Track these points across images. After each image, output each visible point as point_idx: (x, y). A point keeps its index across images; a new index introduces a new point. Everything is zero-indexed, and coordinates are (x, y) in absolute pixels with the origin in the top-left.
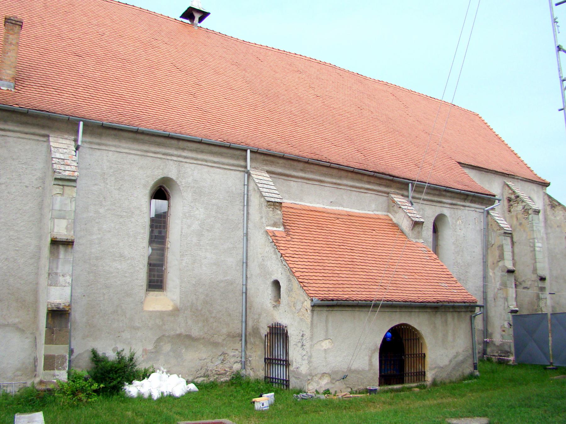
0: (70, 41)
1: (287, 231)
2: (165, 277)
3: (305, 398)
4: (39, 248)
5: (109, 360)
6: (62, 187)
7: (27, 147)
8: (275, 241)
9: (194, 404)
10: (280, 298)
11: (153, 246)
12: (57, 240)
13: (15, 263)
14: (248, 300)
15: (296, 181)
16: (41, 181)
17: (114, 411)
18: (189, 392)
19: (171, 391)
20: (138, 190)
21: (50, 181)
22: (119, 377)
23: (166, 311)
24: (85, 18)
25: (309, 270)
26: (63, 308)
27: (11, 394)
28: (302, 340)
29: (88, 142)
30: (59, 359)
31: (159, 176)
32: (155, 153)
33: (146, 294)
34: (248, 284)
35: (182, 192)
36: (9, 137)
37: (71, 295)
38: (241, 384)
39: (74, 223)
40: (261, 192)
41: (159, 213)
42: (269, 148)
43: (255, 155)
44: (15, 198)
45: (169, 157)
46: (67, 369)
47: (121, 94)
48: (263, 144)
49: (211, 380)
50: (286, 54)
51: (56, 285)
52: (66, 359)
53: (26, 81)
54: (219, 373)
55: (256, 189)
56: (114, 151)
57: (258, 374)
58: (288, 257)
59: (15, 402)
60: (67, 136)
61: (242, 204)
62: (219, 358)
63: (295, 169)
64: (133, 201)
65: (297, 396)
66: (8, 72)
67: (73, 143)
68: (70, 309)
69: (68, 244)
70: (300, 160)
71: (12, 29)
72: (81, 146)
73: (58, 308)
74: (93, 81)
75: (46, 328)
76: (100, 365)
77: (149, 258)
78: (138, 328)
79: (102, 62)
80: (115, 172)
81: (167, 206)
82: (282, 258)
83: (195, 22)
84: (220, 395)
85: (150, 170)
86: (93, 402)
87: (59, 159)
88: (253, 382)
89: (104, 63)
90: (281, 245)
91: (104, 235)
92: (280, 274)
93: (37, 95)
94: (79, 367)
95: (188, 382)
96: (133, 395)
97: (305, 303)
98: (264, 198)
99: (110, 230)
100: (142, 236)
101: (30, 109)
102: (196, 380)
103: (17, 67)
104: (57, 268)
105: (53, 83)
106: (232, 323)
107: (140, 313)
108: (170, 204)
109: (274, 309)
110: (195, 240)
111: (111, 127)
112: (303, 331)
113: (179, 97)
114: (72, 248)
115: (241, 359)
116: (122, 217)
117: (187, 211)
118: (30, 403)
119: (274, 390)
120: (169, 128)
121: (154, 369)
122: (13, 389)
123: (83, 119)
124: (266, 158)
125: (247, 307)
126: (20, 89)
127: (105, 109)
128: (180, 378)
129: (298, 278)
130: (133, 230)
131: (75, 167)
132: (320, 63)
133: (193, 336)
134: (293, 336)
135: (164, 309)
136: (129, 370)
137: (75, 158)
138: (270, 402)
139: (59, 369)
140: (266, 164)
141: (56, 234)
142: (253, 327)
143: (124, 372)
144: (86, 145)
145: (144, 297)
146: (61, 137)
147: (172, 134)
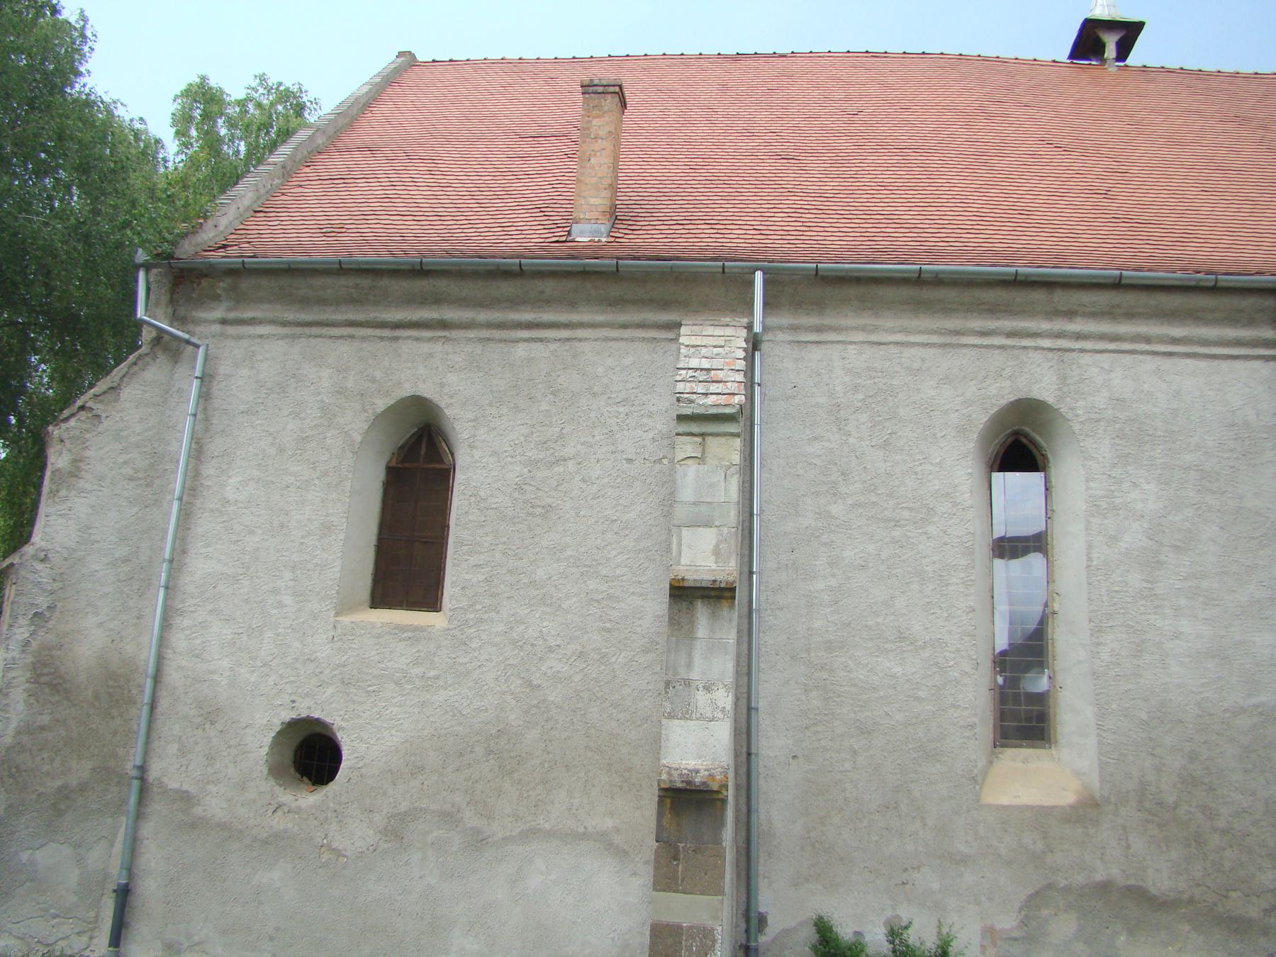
2: (1051, 701)
6: (699, 439)
7: (628, 360)
12: (686, 584)
16: (666, 442)
20: (942, 445)
26: (704, 783)
30: (693, 938)
32: (983, 334)
36: (580, 340)
44: (600, 494)
49: (152, 824)
51: (686, 715)
56: (863, 343)
60: (728, 319)
66: (592, 201)
73: (689, 783)
75: (657, 841)
78: (964, 860)
85: (974, 382)
87: (696, 370)
91: (849, 578)
99: (863, 563)
100: (962, 575)
104: (689, 666)
108: (1050, 482)
110: (1136, 579)
117: (1100, 493)
123: (752, 261)
130: (936, 558)
131: (736, 385)
133: (1153, 891)
135: (1048, 802)
146: (712, 323)
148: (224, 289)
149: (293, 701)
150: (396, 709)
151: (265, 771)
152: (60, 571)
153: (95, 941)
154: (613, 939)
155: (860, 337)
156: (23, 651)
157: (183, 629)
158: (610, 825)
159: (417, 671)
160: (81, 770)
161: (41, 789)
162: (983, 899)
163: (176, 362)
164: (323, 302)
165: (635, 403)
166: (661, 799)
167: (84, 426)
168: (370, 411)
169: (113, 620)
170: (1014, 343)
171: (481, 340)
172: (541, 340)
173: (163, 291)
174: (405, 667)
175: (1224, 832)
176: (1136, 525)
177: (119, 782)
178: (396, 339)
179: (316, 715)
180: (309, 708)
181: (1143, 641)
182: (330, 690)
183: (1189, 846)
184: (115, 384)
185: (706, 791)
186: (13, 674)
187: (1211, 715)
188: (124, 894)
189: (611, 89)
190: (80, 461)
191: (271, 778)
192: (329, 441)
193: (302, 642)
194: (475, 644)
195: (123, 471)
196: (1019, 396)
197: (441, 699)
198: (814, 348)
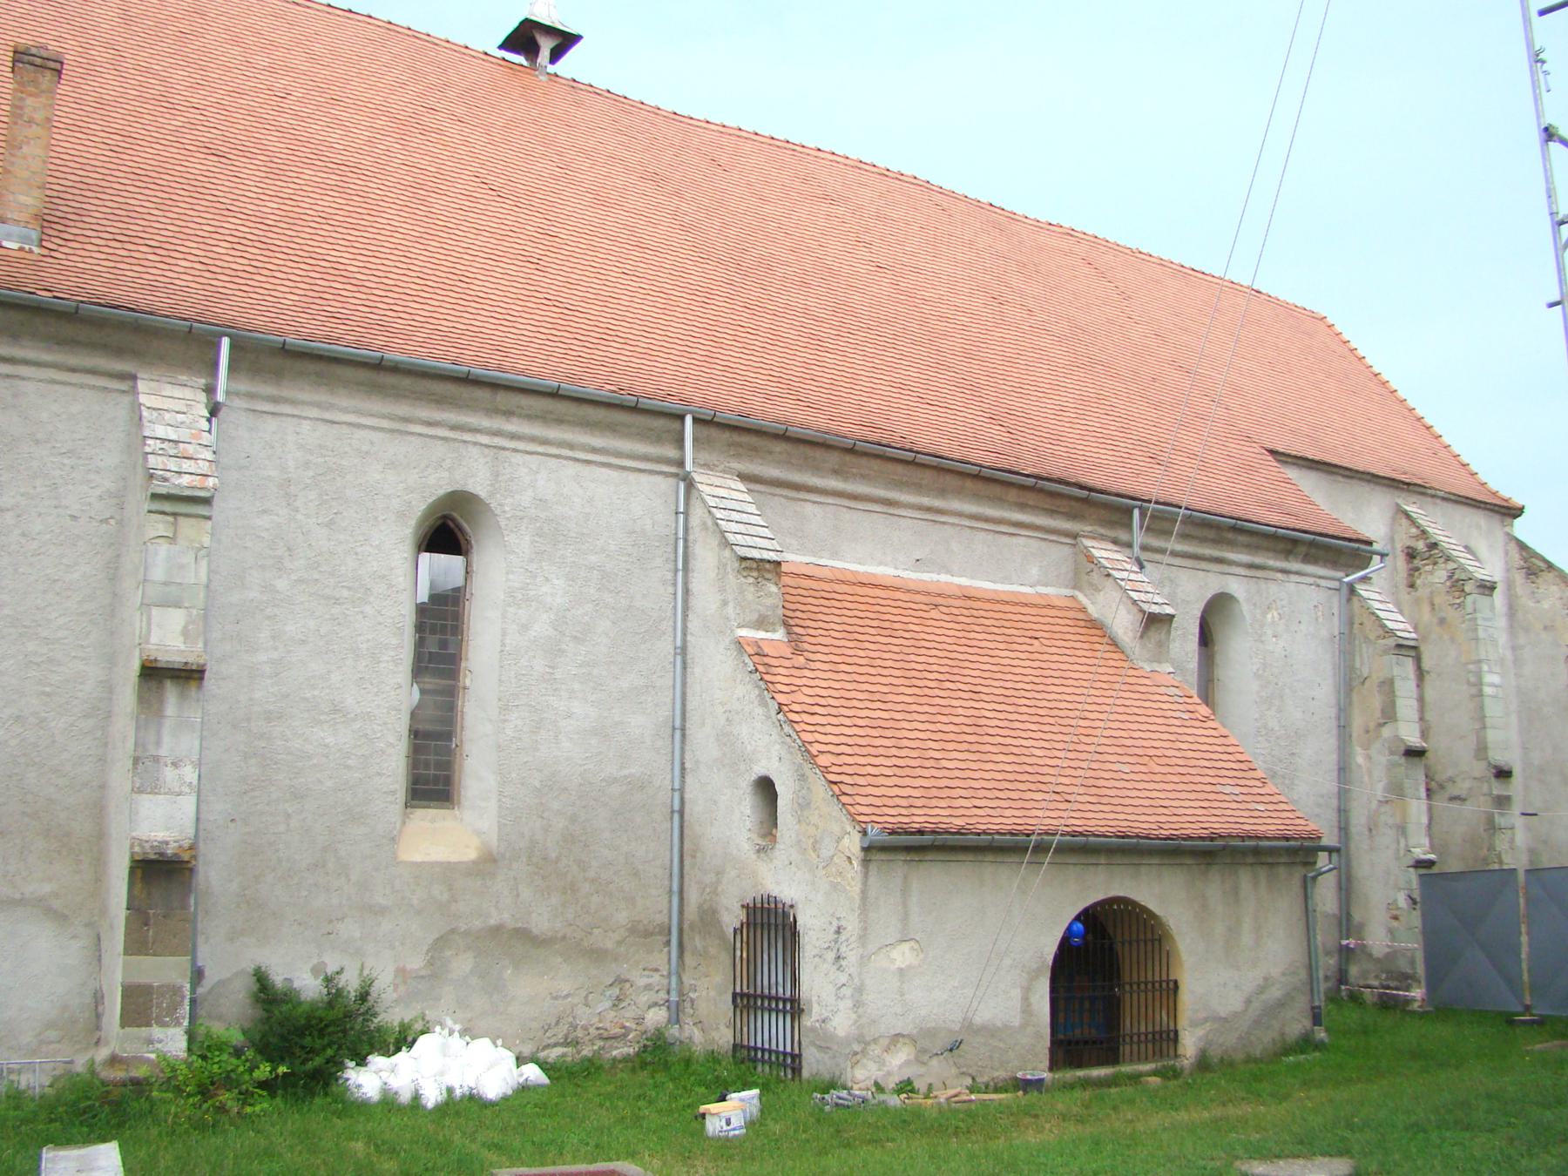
0: (193, 115)
1: (795, 641)
2: (456, 767)
3: (846, 1103)
4: (109, 688)
5: (302, 999)
6: (171, 519)
8: (761, 668)
9: (537, 1121)
10: (775, 825)
11: (424, 683)
12: (159, 665)
13: (42, 728)
14: (686, 831)
15: (821, 503)
16: (114, 501)
17: (316, 1140)
18: (524, 1089)
19: (473, 1086)
21: (138, 502)
22: (330, 1045)
23: (460, 862)
25: (857, 750)
26: (176, 854)
27: (30, 1092)
28: (836, 942)
29: (244, 395)
32: (429, 424)
34: (687, 789)
35: (505, 532)
36: (23, 379)
37: (198, 819)
38: (666, 1066)
39: (205, 617)
40: (723, 533)
41: (439, 590)
42: (745, 409)
43: (706, 431)
44: (42, 550)
45: (467, 437)
46: (186, 1023)
47: (334, 259)
48: (729, 400)
50: (794, 150)
51: (155, 791)
52: (183, 997)
53: (72, 224)
54: (605, 1034)
55: (710, 523)
56: (318, 419)
58: (797, 712)
60: (185, 378)
61: (671, 566)
62: (608, 993)
63: (817, 469)
64: (370, 559)
65: (823, 1098)
66: (22, 199)
67: (202, 397)
68: (194, 857)
69: (189, 675)
71: (34, 82)
72: (224, 405)
73: (161, 854)
76: (276, 1012)
77: (413, 715)
78: (382, 911)
79: (282, 173)
80: (319, 478)
81: (463, 572)
82: (781, 716)
83: (539, 60)
84: (609, 1096)
85: (416, 470)
86: (259, 1116)
87: (163, 440)
88: (701, 1059)
90: (779, 679)
91: (289, 652)
92: (775, 761)
94: (220, 1018)
95: (520, 1060)
96: (369, 1095)
97: (846, 841)
99: (304, 638)
100: (392, 654)
101: (82, 302)
102: (542, 1055)
103: (48, 186)
104: (158, 743)
105: (146, 229)
106: (642, 897)
108: (471, 566)
109: (759, 857)
111: (309, 351)
112: (838, 919)
114: (200, 687)
115: (667, 997)
116: (337, 601)
117: (516, 585)
118: (82, 1118)
119: (760, 1081)
121: (428, 1022)
122: (36, 1080)
123: (229, 329)
124: (736, 437)
126: (55, 247)
128: (501, 1049)
129: (825, 770)
131: (208, 464)
132: (885, 174)
133: (535, 931)
135: (454, 858)
136: (358, 1027)
137: (206, 438)
138: (748, 1115)
139: (164, 1025)
140: (738, 456)
142: (700, 907)
145: (398, 825)
146: (169, 380)
162: (397, 944)
170: (456, 437)
175: (593, 881)
176: (545, 616)
181: (542, 719)
185: (176, 862)
187: (590, 783)
189: (52, 65)
198: (269, 419)
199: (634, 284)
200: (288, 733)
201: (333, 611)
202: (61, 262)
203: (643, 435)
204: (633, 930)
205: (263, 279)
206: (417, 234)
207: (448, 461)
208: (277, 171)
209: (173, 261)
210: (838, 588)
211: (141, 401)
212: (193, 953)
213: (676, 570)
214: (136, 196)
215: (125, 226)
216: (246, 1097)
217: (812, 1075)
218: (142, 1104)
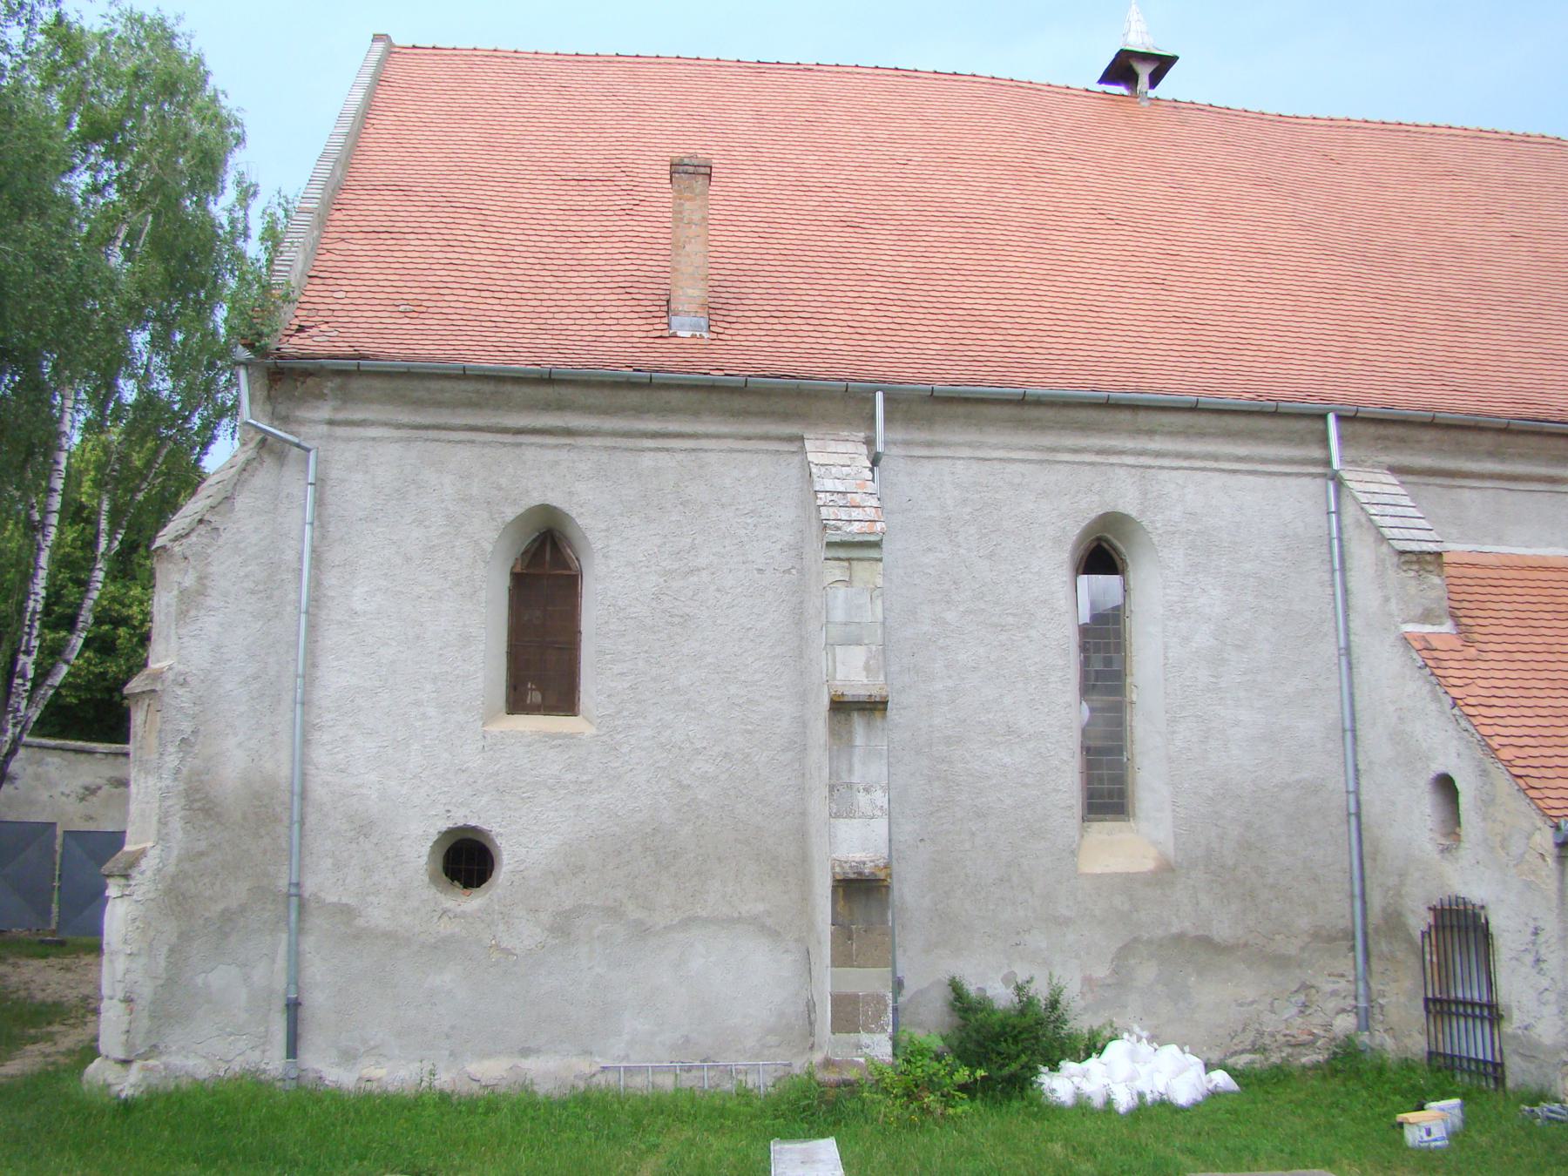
0: (826, 193)
1: (1464, 632)
2: (1130, 780)
3: (1559, 1117)
4: (803, 723)
5: (996, 1007)
6: (846, 564)
7: (753, 472)
8: (1430, 663)
9: (1229, 1127)
10: (1458, 824)
11: (1092, 701)
12: (846, 699)
13: (746, 763)
14: (1364, 833)
15: (1480, 488)
16: (794, 553)
17: (1016, 1141)
18: (1214, 1095)
19: (1162, 1090)
21: (815, 551)
22: (1023, 1051)
23: (1138, 873)
24: (857, 129)
25: (1541, 741)
26: (873, 873)
27: (756, 1091)
28: (1534, 943)
29: (901, 443)
31: (1092, 510)
32: (1076, 451)
33: (1083, 827)
34: (1363, 791)
35: (1160, 549)
36: (706, 451)
37: (890, 841)
38: (1358, 1074)
39: (884, 651)
40: (1378, 528)
41: (1100, 610)
42: (1388, 401)
43: (1350, 428)
45: (1113, 459)
46: (890, 1029)
47: (970, 307)
48: (1372, 394)
50: (1407, 131)
52: (886, 1005)
53: (733, 308)
54: (1293, 1041)
55: (1363, 520)
56: (971, 458)
57: (1409, 1046)
58: (1473, 706)
59: (769, 1112)
60: (846, 433)
61: (1328, 567)
62: (1293, 1000)
63: (1472, 454)
64: (1031, 585)
65: (1533, 1111)
66: (690, 292)
67: (863, 449)
68: (890, 875)
69: (874, 707)
70: (1485, 425)
71: (689, 188)
72: (883, 454)
73: (860, 874)
74: (897, 285)
76: (973, 1021)
77: (1084, 732)
78: (1065, 922)
79: (912, 233)
80: (976, 513)
81: (1120, 590)
82: (1455, 711)
83: (1138, 88)
84: (1300, 1104)
85: (1068, 496)
86: (960, 1117)
87: (832, 493)
88: (1395, 1067)
89: (917, 233)
90: (1450, 672)
91: (963, 679)
92: (1452, 755)
93: (763, 339)
94: (920, 1025)
95: (1209, 1067)
96: (1062, 1099)
97: (1537, 837)
98: (1389, 544)
99: (975, 665)
100: (1060, 674)
101: (750, 376)
102: (1230, 1061)
103: (710, 277)
104: (850, 771)
105: (799, 303)
106: (1323, 902)
107: (1068, 880)
108: (1128, 584)
109: (1443, 857)
111: (957, 395)
112: (1535, 919)
113: (1123, 295)
114: (884, 717)
115: (1353, 1002)
116: (1003, 628)
117: (1176, 599)
118: (802, 1116)
119: (1459, 1090)
120: (1105, 382)
121: (1116, 1029)
122: (761, 1080)
123: (880, 383)
124: (1382, 430)
125: (1364, 851)
126: (721, 330)
127: (934, 352)
128: (1188, 1055)
129: (1509, 764)
131: (874, 510)
132: (1509, 139)
133: (1217, 939)
134: (1505, 934)
136: (1049, 1034)
137: (871, 488)
138: (1450, 1125)
139: (871, 1031)
140: (1386, 448)
141: (844, 685)
142: (1384, 909)
143: (1037, 1038)
144: (895, 451)
145: (1076, 838)
146: (832, 437)
147: (1116, 395)
148: (332, 390)
149: (449, 811)
150: (552, 814)
151: (427, 879)
152: (199, 694)
153: (268, 1054)
154: (770, 1009)
155: (967, 452)
156: (176, 779)
157: (323, 744)
158: (762, 909)
159: (569, 776)
160: (239, 891)
161: (207, 914)
163: (282, 465)
164: (439, 404)
165: (763, 514)
166: (835, 889)
167: (205, 541)
168: (499, 520)
169: (250, 739)
171: (606, 448)
172: (667, 450)
173: (257, 385)
174: (558, 773)
177: (274, 900)
178: (519, 445)
179: (473, 823)
180: (465, 816)
182: (485, 799)
183: (1245, 900)
184: (229, 494)
185: (873, 880)
186: (169, 802)
188: (293, 1008)
189: (702, 170)
190: (206, 578)
191: (432, 886)
192: (457, 550)
193: (451, 754)
194: (625, 749)
195: (245, 585)
196: (1108, 509)
197: (596, 802)
198: (925, 462)
199: (1260, 290)
200: (967, 755)
201: (1000, 638)
202: (728, 343)
203: (1287, 439)
204: (1316, 936)
205: (907, 334)
206: (1045, 272)
207: (1097, 485)
208: (908, 233)
209: (825, 329)
210: (1505, 574)
211: (810, 459)
212: (893, 964)
213: (1333, 571)
214: (785, 274)
215: (779, 303)
216: (947, 1100)
217: (1517, 1085)
218: (852, 1105)
